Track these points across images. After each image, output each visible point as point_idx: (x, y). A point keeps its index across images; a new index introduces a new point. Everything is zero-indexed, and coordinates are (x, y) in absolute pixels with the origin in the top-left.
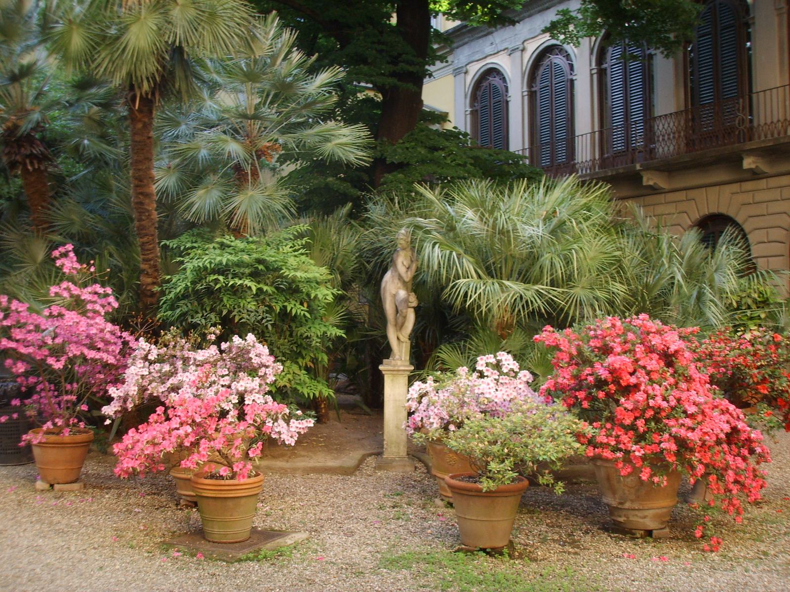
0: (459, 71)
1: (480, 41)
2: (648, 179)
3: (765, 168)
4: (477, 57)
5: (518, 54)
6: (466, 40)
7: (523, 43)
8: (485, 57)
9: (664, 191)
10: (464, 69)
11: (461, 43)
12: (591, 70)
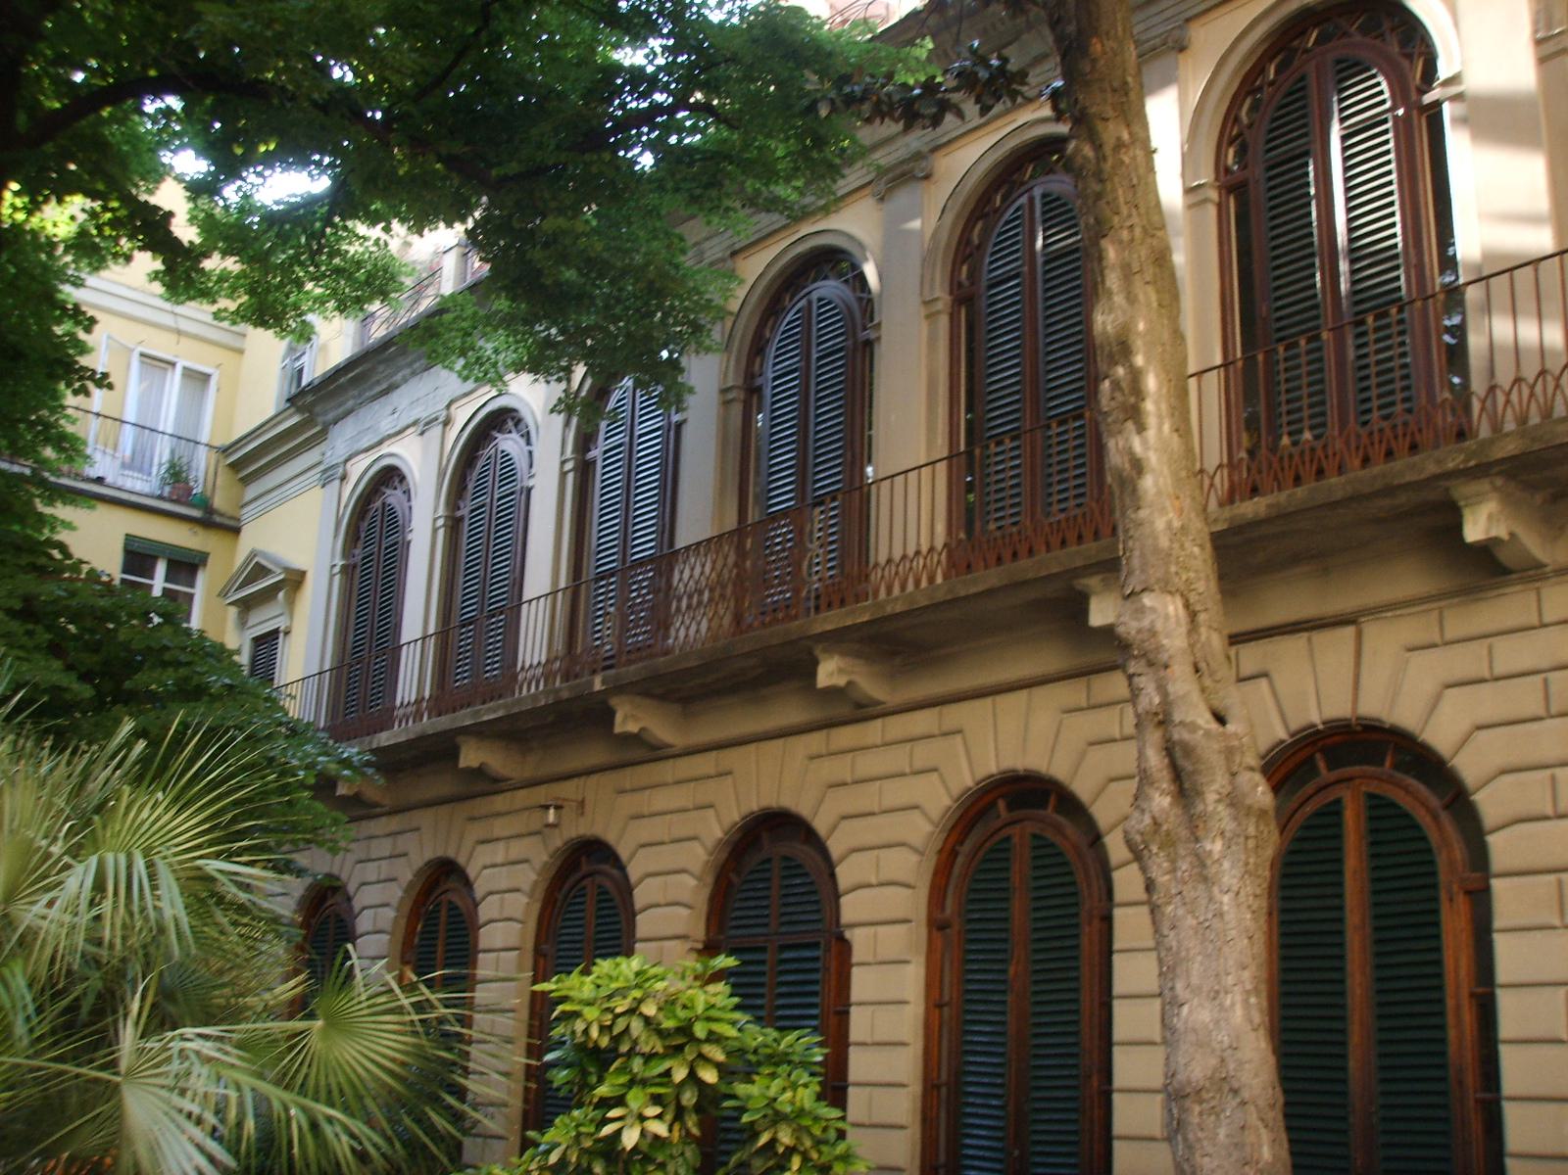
0: (332, 475)
1: (376, 405)
2: (625, 718)
3: (871, 685)
4: (365, 444)
5: (436, 431)
6: (350, 403)
7: (448, 406)
8: (380, 443)
9: (670, 751)
10: (340, 470)
11: (341, 410)
12: (563, 463)
